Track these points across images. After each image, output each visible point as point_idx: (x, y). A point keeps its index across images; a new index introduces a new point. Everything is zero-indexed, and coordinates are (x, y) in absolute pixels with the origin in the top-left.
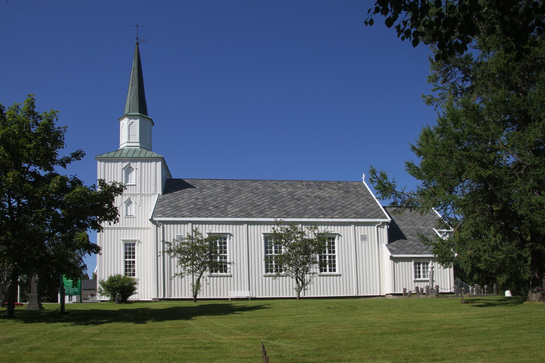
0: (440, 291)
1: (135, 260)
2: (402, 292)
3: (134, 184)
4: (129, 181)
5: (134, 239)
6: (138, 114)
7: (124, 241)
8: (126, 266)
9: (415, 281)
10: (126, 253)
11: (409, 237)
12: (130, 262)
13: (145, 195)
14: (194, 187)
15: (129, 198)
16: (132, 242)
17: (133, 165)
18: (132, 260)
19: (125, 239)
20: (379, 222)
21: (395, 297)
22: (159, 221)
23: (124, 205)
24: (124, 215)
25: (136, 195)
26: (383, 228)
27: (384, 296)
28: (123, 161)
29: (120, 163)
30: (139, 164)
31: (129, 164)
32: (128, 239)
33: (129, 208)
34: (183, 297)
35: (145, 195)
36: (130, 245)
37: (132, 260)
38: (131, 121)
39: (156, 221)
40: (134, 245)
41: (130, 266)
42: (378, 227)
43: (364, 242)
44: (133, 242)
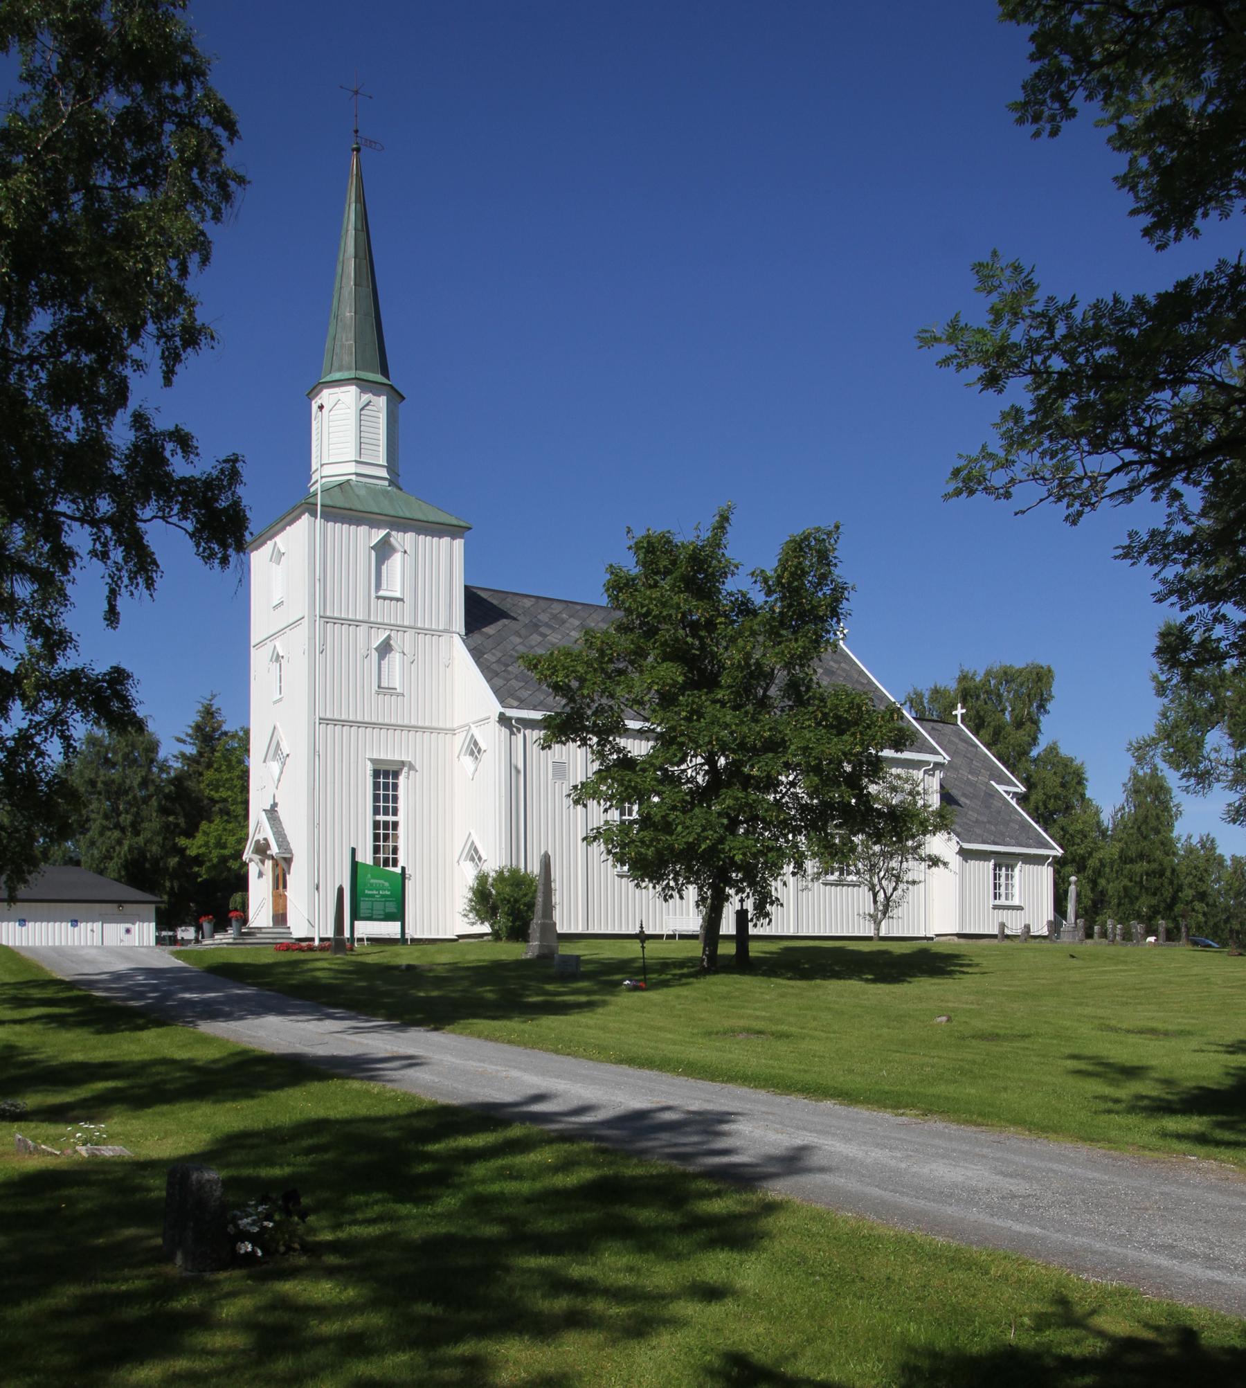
0: (1007, 932)
1: (401, 818)
2: (996, 932)
3: (398, 595)
4: (384, 586)
5: (397, 758)
6: (352, 374)
7: (374, 761)
8: (376, 837)
9: (995, 907)
10: (376, 798)
11: (962, 800)
12: (386, 824)
13: (336, 621)
14: (515, 619)
15: (389, 637)
16: (392, 768)
17: (398, 538)
18: (381, 818)
19: (375, 756)
20: (928, 763)
21: (962, 941)
22: (519, 720)
23: (375, 655)
24: (375, 687)
25: (402, 628)
26: (933, 775)
27: (932, 939)
28: (374, 524)
29: (363, 529)
30: (410, 536)
31: (388, 535)
32: (383, 757)
33: (385, 663)
34: (616, 931)
35: (336, 621)
36: (386, 774)
37: (390, 818)
38: (366, 397)
39: (510, 719)
40: (396, 775)
41: (386, 837)
42: (925, 772)
43: (559, 782)
44: (395, 768)
